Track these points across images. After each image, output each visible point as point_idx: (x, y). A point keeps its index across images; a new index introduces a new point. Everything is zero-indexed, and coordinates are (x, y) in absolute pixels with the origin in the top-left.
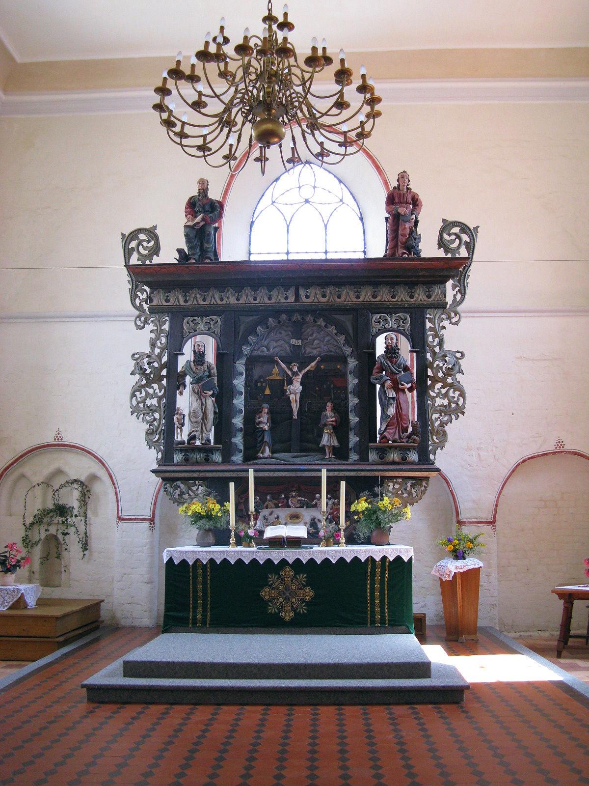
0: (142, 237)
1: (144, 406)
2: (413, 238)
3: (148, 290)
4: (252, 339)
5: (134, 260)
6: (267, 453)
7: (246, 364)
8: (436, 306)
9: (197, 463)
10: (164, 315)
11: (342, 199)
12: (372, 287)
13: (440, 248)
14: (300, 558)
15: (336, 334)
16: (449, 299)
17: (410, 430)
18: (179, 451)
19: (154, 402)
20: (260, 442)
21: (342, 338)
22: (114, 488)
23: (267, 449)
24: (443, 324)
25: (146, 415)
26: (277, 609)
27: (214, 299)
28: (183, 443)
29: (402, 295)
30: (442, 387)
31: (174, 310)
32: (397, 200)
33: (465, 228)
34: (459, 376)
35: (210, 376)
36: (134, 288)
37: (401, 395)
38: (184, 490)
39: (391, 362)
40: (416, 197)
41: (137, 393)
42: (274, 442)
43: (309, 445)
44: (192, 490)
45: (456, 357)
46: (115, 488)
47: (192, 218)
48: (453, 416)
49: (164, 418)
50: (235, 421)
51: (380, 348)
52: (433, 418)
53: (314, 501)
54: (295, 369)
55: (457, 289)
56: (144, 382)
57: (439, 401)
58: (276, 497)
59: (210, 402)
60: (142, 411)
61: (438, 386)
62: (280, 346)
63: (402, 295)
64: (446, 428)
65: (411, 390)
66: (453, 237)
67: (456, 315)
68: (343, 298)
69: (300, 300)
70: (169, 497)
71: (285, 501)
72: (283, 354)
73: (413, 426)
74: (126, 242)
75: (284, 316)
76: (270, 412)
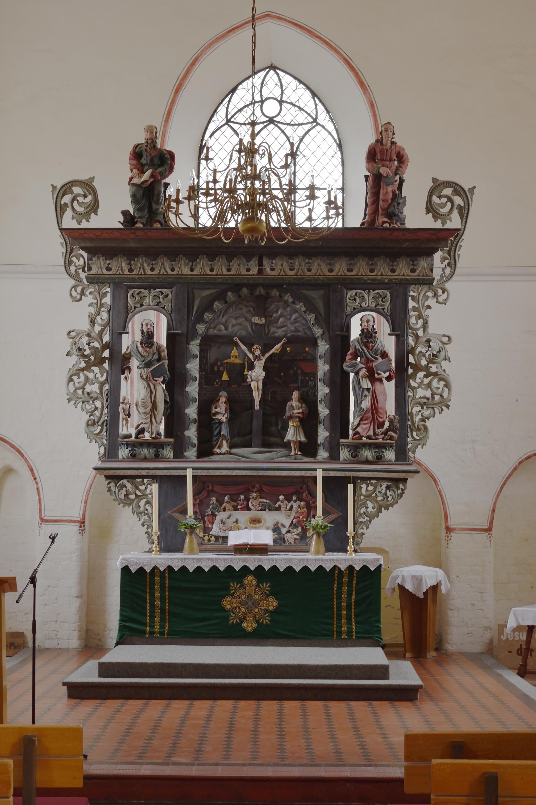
0: (77, 190)
1: (83, 392)
2: (396, 204)
3: (85, 255)
4: (208, 316)
5: (69, 222)
6: (225, 448)
7: (200, 345)
8: (421, 282)
9: (145, 459)
10: (105, 286)
11: (317, 117)
12: (348, 259)
13: (429, 213)
14: (262, 565)
15: (305, 312)
16: (437, 274)
17: (387, 425)
18: (124, 446)
19: (95, 388)
20: (217, 435)
21: (311, 318)
22: (35, 483)
23: (225, 443)
24: (429, 302)
25: (85, 403)
26: (239, 619)
27: (165, 269)
28: (130, 436)
29: (382, 269)
30: (426, 376)
31: (117, 280)
32: (378, 156)
33: (458, 190)
34: (445, 364)
35: (159, 360)
36: (69, 252)
37: (378, 385)
38: (130, 490)
39: (367, 347)
40: (402, 152)
41: (75, 378)
42: (233, 435)
43: (273, 440)
44: (139, 490)
45: (442, 342)
46: (37, 483)
47: (139, 174)
48: (436, 410)
49: (107, 408)
50: (187, 411)
51: (355, 333)
52: (414, 411)
53: (278, 503)
54: (258, 353)
55: (446, 262)
56: (83, 365)
57: (421, 393)
58: (234, 498)
59: (161, 389)
60: (80, 398)
61: (421, 374)
62: (240, 324)
63: (382, 269)
64: (428, 423)
65: (389, 379)
66: (444, 200)
67: (444, 293)
68: (313, 271)
69: (264, 272)
70: (113, 497)
71: (245, 503)
72: (244, 333)
73: (391, 421)
74: (57, 196)
75: (245, 290)
76: (229, 401)
